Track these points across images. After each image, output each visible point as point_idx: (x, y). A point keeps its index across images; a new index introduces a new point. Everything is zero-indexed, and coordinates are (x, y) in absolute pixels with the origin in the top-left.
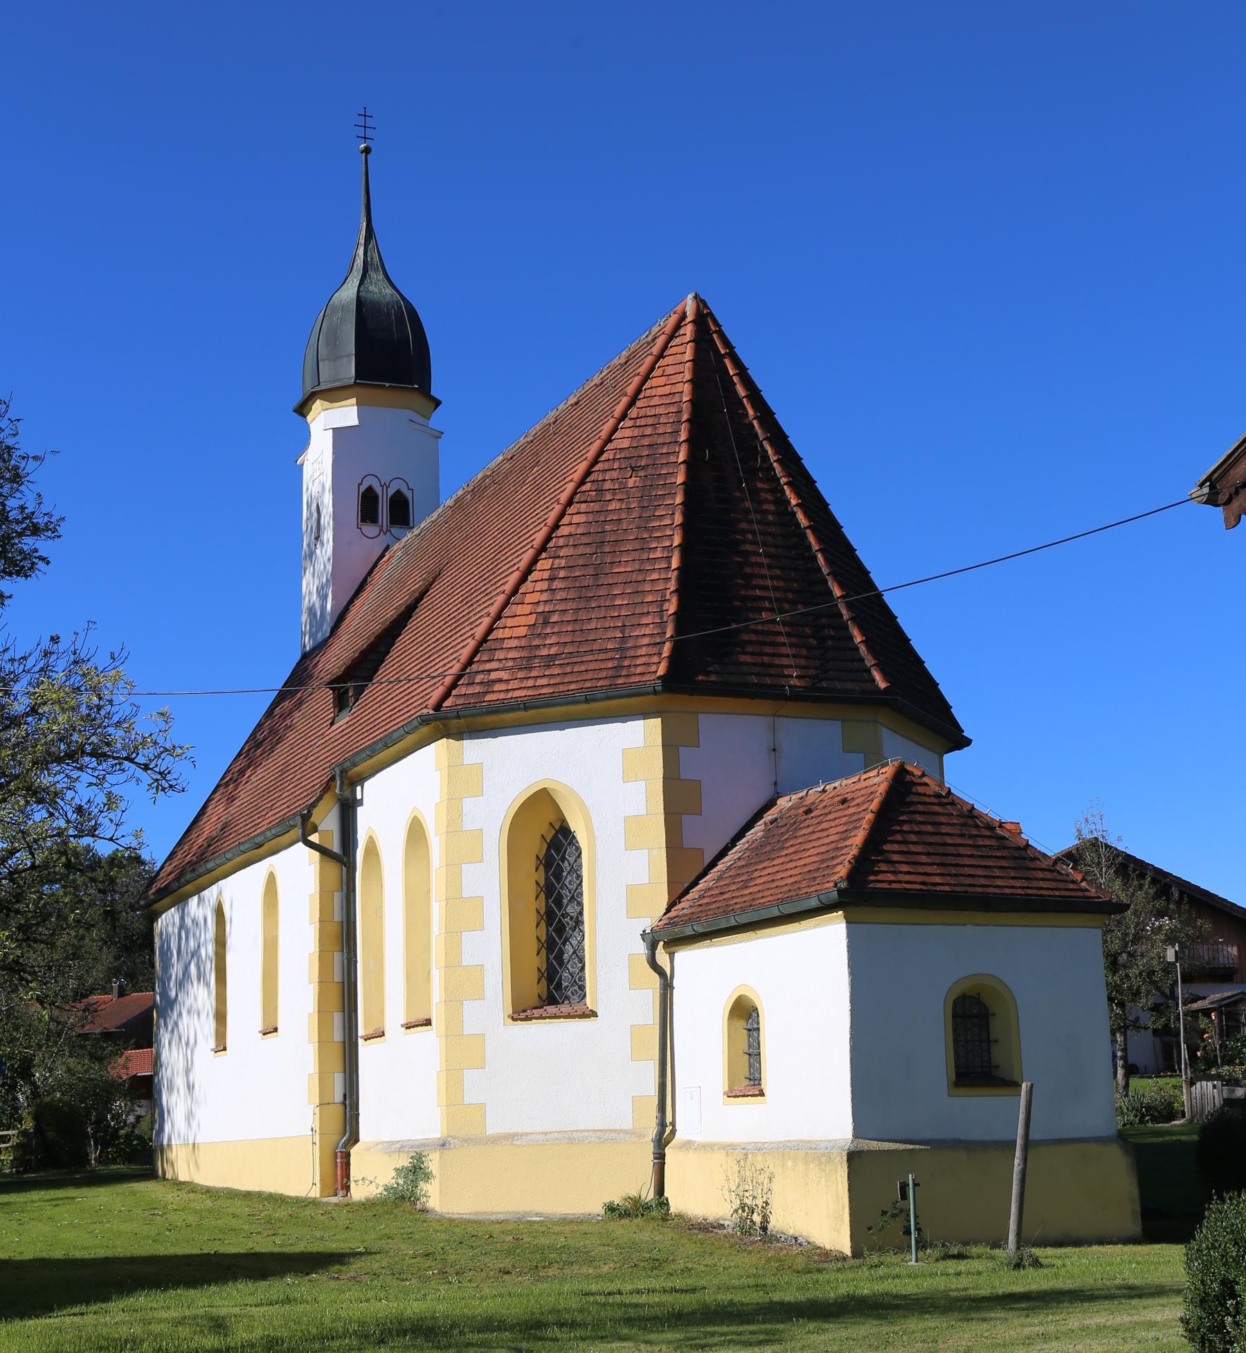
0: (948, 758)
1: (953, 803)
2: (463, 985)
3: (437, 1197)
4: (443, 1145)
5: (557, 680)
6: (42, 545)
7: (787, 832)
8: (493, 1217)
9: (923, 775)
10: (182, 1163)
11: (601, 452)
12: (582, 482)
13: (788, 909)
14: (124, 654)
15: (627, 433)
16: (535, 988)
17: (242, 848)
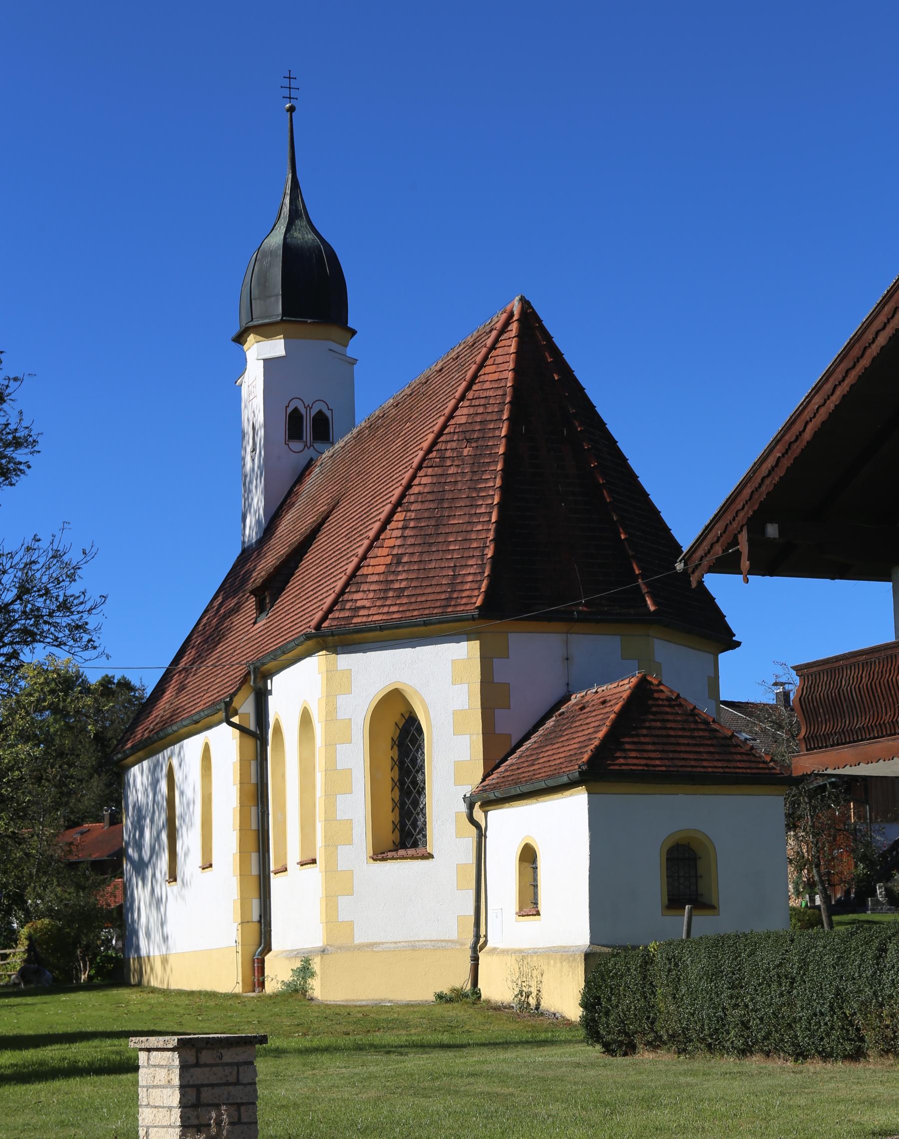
0: (722, 657)
1: (680, 705)
2: (338, 835)
3: (318, 989)
4: (323, 951)
5: (405, 608)
6: (20, 455)
7: (567, 723)
8: (358, 1003)
9: (660, 684)
10: (156, 979)
11: (445, 426)
12: (429, 451)
13: (551, 783)
14: (94, 550)
15: (465, 411)
16: (390, 836)
17: (184, 723)
